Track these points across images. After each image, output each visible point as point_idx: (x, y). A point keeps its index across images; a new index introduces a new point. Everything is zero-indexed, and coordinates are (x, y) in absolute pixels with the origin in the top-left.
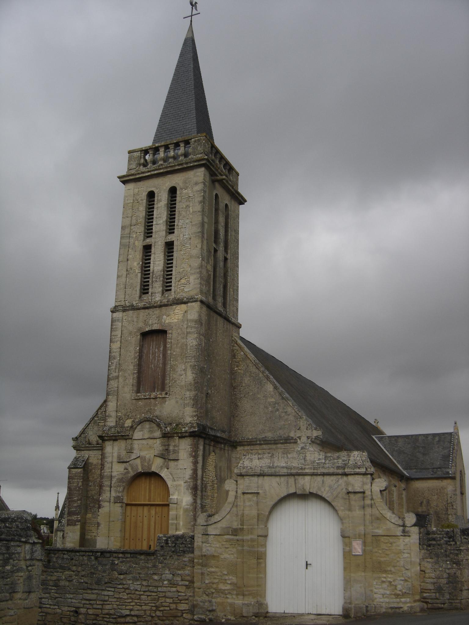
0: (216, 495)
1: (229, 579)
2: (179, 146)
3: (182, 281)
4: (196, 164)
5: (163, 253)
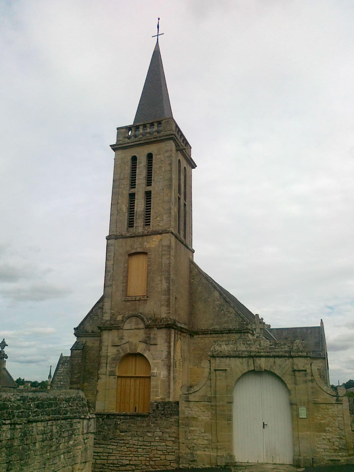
0: (181, 370)
1: (206, 436)
2: (154, 125)
3: (157, 218)
4: (166, 137)
5: (144, 199)
